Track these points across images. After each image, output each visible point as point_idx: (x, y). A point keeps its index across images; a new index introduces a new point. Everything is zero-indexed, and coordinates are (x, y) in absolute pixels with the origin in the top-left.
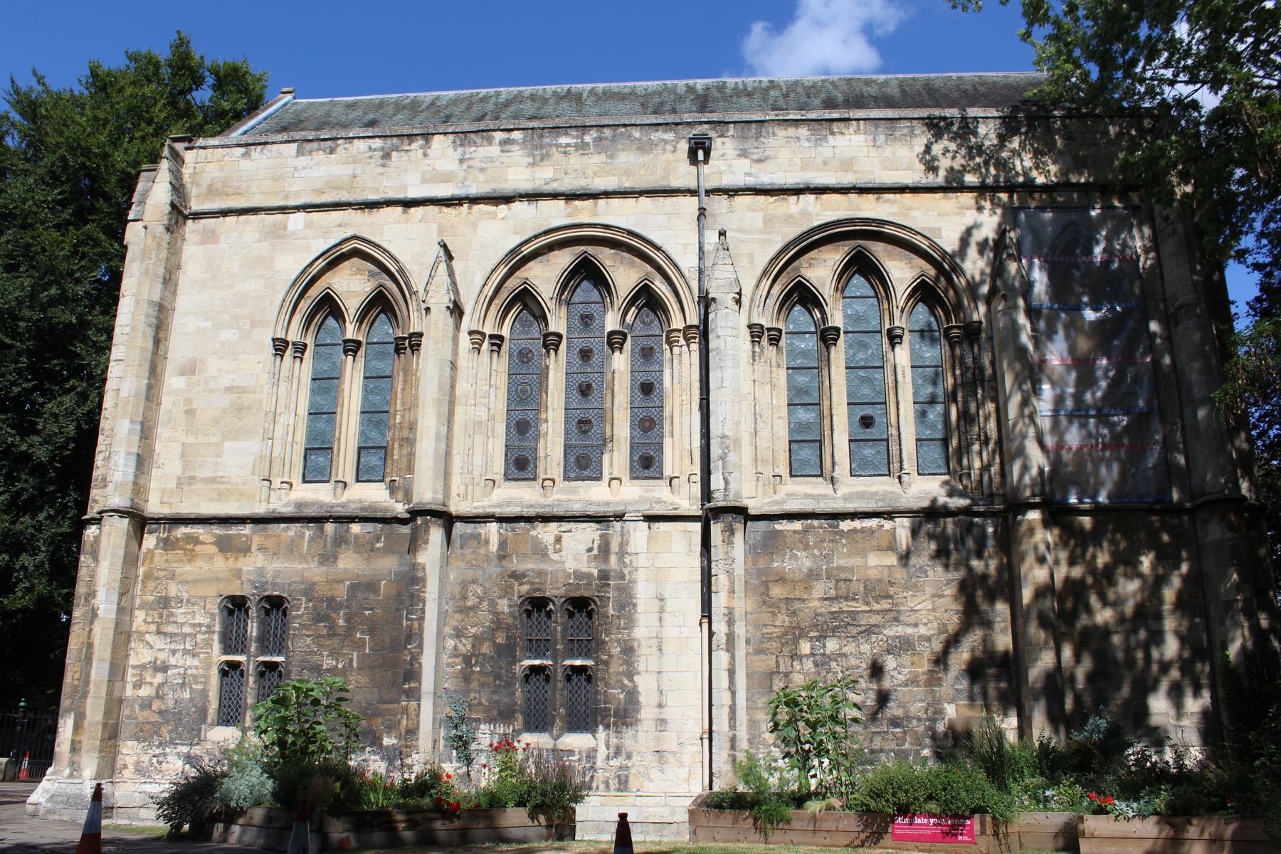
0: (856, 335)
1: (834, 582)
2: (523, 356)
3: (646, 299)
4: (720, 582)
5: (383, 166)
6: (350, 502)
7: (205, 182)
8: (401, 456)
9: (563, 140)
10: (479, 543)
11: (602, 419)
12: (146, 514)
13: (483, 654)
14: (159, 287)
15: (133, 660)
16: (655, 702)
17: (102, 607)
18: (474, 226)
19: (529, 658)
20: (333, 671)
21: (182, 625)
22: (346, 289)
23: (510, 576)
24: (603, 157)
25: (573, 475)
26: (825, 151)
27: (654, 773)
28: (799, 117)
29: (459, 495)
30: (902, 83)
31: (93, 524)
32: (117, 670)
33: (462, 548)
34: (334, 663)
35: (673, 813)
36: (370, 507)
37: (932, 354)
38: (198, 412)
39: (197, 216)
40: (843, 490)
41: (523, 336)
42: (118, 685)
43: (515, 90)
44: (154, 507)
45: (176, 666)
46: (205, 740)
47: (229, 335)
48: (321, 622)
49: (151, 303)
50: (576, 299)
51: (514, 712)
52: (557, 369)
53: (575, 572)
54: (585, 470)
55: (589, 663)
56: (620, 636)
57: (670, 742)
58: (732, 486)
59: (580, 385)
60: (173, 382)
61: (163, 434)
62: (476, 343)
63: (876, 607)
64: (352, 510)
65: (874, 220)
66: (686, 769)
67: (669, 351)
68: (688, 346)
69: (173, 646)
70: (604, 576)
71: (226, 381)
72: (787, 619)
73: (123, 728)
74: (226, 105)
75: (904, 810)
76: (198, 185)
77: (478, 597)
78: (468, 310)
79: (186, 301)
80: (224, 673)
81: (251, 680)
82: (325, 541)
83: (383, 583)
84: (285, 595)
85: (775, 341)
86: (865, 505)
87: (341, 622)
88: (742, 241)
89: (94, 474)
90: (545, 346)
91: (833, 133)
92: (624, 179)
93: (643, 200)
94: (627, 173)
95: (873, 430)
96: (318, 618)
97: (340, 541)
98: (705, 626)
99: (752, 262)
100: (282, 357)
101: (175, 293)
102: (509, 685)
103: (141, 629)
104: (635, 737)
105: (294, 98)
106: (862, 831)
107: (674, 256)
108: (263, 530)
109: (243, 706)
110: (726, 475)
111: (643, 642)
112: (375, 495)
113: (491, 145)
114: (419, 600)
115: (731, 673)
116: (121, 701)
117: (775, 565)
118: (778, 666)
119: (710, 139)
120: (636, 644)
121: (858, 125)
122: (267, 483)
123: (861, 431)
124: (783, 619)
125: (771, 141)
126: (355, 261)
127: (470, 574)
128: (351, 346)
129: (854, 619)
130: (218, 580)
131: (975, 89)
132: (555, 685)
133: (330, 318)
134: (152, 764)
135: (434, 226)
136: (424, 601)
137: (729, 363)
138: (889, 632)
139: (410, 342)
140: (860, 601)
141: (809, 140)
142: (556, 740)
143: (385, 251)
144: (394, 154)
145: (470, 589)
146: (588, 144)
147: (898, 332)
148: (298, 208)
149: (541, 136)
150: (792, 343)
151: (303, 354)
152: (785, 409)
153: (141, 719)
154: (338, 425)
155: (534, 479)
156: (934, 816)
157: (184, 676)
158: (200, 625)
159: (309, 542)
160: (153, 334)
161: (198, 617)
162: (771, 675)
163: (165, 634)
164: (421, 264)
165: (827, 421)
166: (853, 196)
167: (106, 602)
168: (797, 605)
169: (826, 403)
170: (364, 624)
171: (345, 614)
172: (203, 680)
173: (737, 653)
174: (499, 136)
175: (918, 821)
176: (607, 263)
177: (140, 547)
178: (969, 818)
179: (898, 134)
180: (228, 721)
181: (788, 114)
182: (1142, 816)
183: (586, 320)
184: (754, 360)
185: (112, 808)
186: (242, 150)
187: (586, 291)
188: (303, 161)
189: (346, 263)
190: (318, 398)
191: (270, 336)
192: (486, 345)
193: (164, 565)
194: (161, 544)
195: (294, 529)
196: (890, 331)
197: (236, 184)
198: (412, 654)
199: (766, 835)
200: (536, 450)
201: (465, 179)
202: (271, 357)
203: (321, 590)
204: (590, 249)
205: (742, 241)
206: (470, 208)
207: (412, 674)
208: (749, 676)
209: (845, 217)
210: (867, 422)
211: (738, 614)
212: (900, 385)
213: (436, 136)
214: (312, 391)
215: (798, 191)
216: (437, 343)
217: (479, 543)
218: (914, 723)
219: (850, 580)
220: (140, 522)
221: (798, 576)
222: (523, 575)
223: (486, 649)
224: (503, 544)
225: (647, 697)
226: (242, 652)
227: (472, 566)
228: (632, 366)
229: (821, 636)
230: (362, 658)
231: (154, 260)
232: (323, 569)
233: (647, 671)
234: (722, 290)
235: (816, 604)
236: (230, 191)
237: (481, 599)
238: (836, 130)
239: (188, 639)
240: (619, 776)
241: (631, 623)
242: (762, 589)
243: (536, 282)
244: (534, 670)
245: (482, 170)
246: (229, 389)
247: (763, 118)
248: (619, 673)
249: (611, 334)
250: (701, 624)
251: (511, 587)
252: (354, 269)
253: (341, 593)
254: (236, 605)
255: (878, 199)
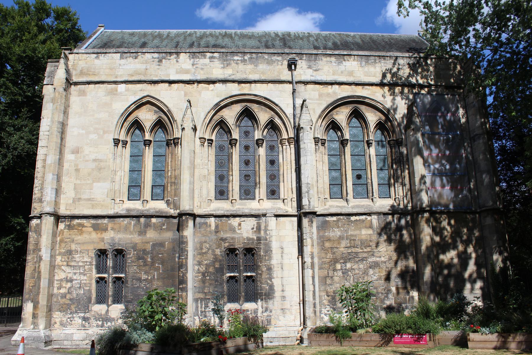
0: (354, 142)
1: (349, 241)
2: (221, 148)
3: (272, 126)
4: (308, 242)
5: (159, 65)
6: (150, 209)
7: (79, 69)
8: (171, 190)
9: (236, 58)
10: (207, 226)
11: (255, 175)
12: (59, 214)
13: (210, 272)
14: (62, 115)
15: (56, 278)
16: (280, 289)
17: (44, 255)
18: (200, 93)
19: (228, 273)
20: (146, 280)
21: (78, 262)
22: (144, 118)
23: (220, 240)
24: (252, 66)
25: (243, 198)
26: (342, 67)
27: (281, 318)
28: (331, 53)
29: (197, 206)
30: (361, 36)
31: (35, 219)
32: (51, 282)
33: (199, 228)
34: (147, 277)
35: (289, 333)
36: (159, 211)
37: (382, 151)
38: (81, 170)
39: (76, 84)
40: (351, 204)
41: (220, 140)
42: (51, 288)
43: (203, 31)
44: (63, 211)
45: (76, 280)
46: (91, 310)
47: (93, 136)
48: (140, 260)
49: (59, 122)
50: (242, 125)
51: (224, 295)
52: (236, 153)
53: (247, 238)
54: (248, 195)
55: (254, 274)
56: (266, 263)
57: (287, 305)
58: (312, 203)
59: (245, 161)
60: (69, 157)
61: (65, 179)
62: (202, 143)
63: (365, 250)
64: (151, 212)
65: (362, 97)
66: (294, 315)
67: (281, 147)
68: (290, 146)
69: (75, 271)
70: (259, 239)
71: (93, 157)
72: (331, 255)
73: (53, 307)
74: (62, 27)
75: (398, 332)
76: (75, 70)
77: (207, 248)
78: (198, 128)
79: (71, 122)
80: (97, 282)
81: (110, 284)
82: (141, 226)
83: (167, 243)
84: (124, 249)
85: (323, 144)
86: (360, 210)
87: (149, 260)
88: (311, 103)
89: (34, 197)
90: (230, 144)
91: (345, 60)
92: (262, 75)
93: (270, 84)
94: (263, 73)
95: (361, 180)
96: (139, 258)
97: (147, 226)
98: (300, 259)
99: (314, 112)
100: (117, 146)
101: (67, 118)
102: (221, 284)
103: (59, 264)
104: (273, 304)
105: (105, 29)
106: (381, 341)
107: (283, 109)
108: (113, 221)
109: (107, 295)
110: (309, 199)
111: (275, 266)
112: (160, 206)
113: (205, 58)
114: (185, 250)
115: (313, 278)
116: (52, 295)
117: (326, 234)
118: (328, 274)
119: (297, 60)
120: (272, 266)
121: (354, 57)
122: (113, 201)
123: (357, 180)
124: (330, 255)
125: (320, 62)
126: (148, 106)
127: (204, 239)
128: (147, 142)
129: (357, 255)
130: (93, 242)
131: (390, 41)
132: (240, 284)
133: (137, 130)
134: (67, 322)
135: (183, 93)
136: (187, 251)
137: (309, 154)
138: (370, 260)
139: (174, 142)
140: (359, 248)
141: (335, 63)
142: (241, 306)
143: (162, 102)
144: (164, 60)
145: (204, 245)
146: (246, 60)
147: (371, 141)
148: (122, 82)
149: (227, 56)
150: (329, 145)
151: (126, 145)
152: (327, 172)
153: (61, 302)
154: (143, 176)
155: (228, 199)
156: (411, 334)
157: (80, 284)
158: (86, 262)
159: (134, 226)
160: (60, 136)
161: (85, 258)
162: (326, 277)
163: (71, 266)
164: (178, 108)
165: (344, 177)
166: (353, 86)
167: (46, 253)
168: (335, 250)
169: (344, 169)
170: (159, 260)
171: (151, 256)
172: (89, 285)
173: (315, 270)
174: (208, 55)
175: (404, 336)
176: (256, 110)
177: (57, 227)
178: (425, 335)
179: (370, 62)
180: (100, 302)
181: (327, 51)
182: (491, 333)
183: (247, 133)
184: (316, 152)
185: (52, 341)
186: (95, 55)
187: (247, 122)
188: (123, 61)
189: (144, 106)
190: (133, 164)
191: (112, 138)
192: (206, 144)
193: (69, 236)
194: (67, 227)
195: (127, 220)
196: (367, 141)
197: (93, 70)
198: (183, 273)
199: (341, 343)
200: (228, 187)
201: (195, 72)
202: (113, 147)
203: (140, 246)
204: (249, 104)
205: (311, 103)
206: (198, 85)
207: (183, 281)
208: (319, 277)
209: (351, 95)
210: (359, 177)
211: (315, 254)
212: (372, 162)
213: (182, 53)
214: (130, 161)
215: (332, 84)
216: (188, 143)
217: (207, 226)
218: (380, 295)
219: (355, 240)
220: (58, 218)
221: (336, 238)
222: (226, 239)
223: (211, 269)
224: (217, 226)
225: (277, 288)
226: (105, 273)
227: (204, 236)
228: (266, 153)
229: (345, 262)
230: (159, 274)
231: (59, 103)
232: (140, 237)
233: (277, 277)
234: (305, 124)
235: (342, 249)
236: (91, 73)
237: (209, 249)
238: (346, 59)
239: (81, 268)
240: (267, 319)
241: (270, 258)
242: (321, 244)
243: (226, 117)
244: (231, 277)
245: (202, 69)
246: (95, 160)
247: (317, 53)
248: (266, 278)
249: (257, 140)
250: (298, 258)
251: (221, 244)
252: (148, 109)
253: (149, 247)
254: (102, 253)
255: (363, 88)
